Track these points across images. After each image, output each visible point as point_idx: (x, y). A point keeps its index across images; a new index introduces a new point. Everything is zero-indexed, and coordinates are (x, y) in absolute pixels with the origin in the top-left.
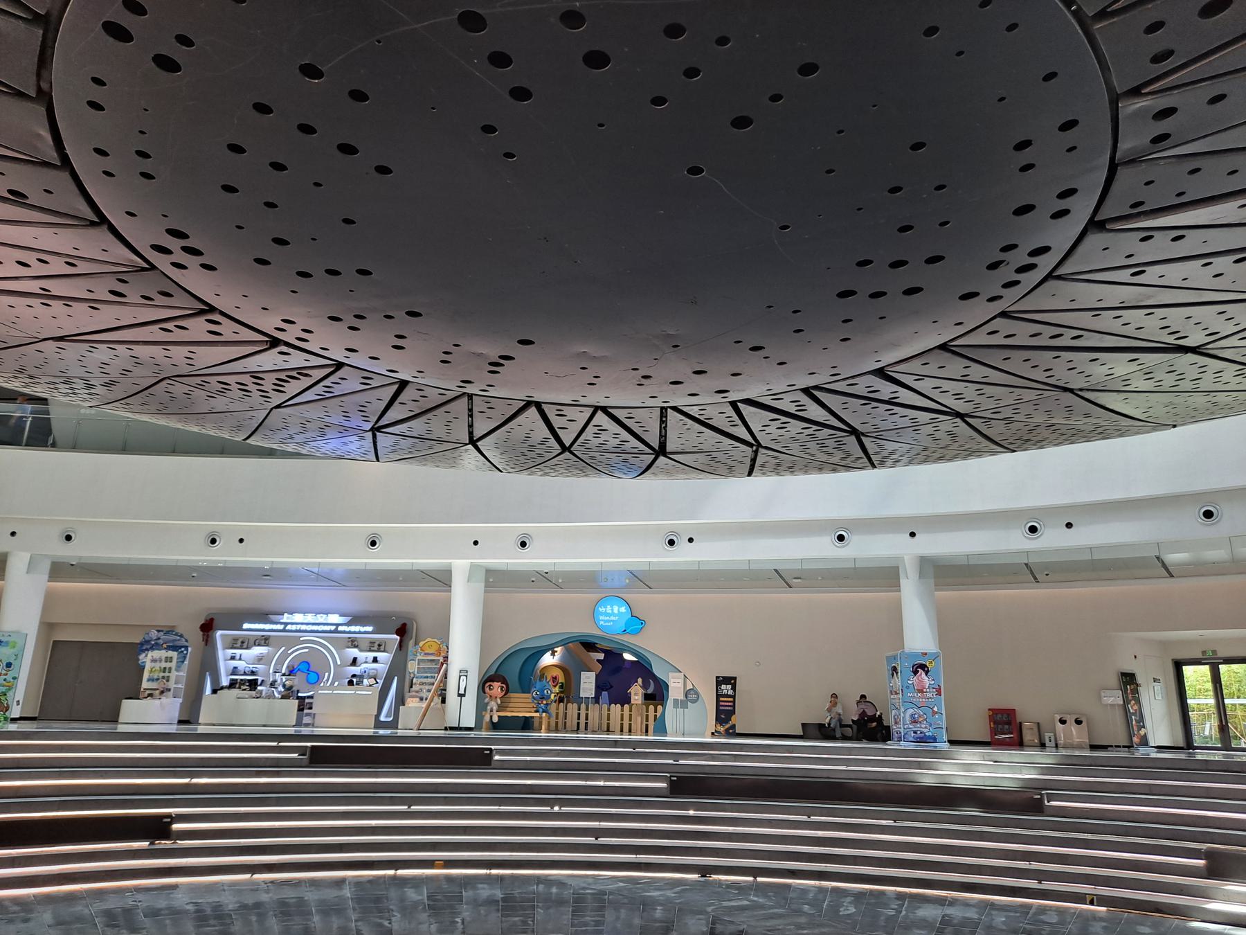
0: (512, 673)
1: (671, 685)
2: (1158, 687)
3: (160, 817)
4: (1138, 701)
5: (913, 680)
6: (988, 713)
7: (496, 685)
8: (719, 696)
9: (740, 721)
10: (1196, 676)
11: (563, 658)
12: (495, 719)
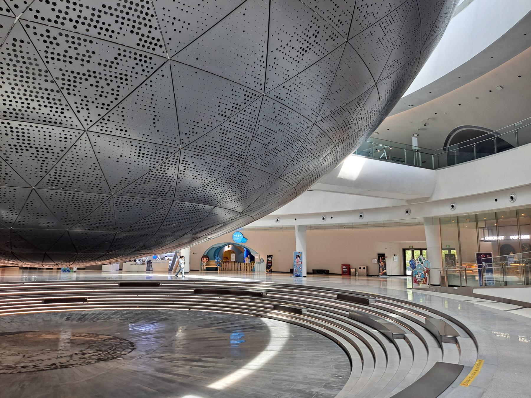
0: (211, 255)
1: (255, 258)
2: (395, 257)
3: (84, 298)
4: (385, 262)
5: (296, 260)
6: (341, 266)
7: (205, 258)
8: (267, 261)
9: (273, 268)
10: (409, 254)
11: (232, 248)
12: (205, 268)
